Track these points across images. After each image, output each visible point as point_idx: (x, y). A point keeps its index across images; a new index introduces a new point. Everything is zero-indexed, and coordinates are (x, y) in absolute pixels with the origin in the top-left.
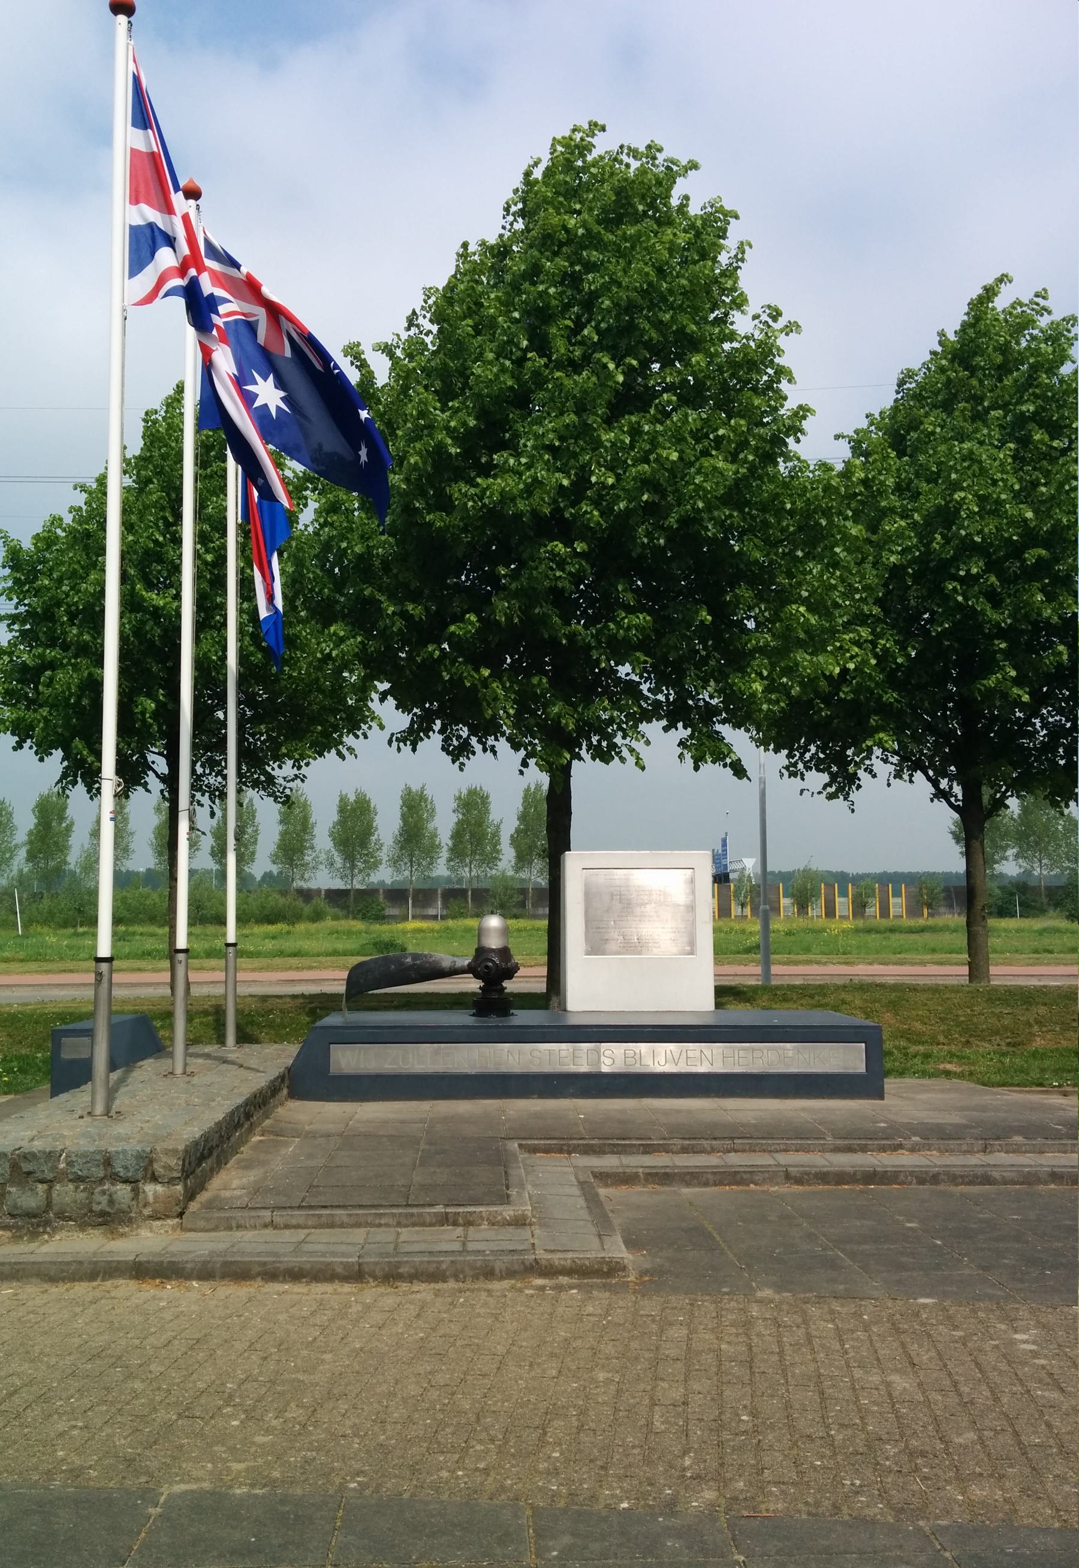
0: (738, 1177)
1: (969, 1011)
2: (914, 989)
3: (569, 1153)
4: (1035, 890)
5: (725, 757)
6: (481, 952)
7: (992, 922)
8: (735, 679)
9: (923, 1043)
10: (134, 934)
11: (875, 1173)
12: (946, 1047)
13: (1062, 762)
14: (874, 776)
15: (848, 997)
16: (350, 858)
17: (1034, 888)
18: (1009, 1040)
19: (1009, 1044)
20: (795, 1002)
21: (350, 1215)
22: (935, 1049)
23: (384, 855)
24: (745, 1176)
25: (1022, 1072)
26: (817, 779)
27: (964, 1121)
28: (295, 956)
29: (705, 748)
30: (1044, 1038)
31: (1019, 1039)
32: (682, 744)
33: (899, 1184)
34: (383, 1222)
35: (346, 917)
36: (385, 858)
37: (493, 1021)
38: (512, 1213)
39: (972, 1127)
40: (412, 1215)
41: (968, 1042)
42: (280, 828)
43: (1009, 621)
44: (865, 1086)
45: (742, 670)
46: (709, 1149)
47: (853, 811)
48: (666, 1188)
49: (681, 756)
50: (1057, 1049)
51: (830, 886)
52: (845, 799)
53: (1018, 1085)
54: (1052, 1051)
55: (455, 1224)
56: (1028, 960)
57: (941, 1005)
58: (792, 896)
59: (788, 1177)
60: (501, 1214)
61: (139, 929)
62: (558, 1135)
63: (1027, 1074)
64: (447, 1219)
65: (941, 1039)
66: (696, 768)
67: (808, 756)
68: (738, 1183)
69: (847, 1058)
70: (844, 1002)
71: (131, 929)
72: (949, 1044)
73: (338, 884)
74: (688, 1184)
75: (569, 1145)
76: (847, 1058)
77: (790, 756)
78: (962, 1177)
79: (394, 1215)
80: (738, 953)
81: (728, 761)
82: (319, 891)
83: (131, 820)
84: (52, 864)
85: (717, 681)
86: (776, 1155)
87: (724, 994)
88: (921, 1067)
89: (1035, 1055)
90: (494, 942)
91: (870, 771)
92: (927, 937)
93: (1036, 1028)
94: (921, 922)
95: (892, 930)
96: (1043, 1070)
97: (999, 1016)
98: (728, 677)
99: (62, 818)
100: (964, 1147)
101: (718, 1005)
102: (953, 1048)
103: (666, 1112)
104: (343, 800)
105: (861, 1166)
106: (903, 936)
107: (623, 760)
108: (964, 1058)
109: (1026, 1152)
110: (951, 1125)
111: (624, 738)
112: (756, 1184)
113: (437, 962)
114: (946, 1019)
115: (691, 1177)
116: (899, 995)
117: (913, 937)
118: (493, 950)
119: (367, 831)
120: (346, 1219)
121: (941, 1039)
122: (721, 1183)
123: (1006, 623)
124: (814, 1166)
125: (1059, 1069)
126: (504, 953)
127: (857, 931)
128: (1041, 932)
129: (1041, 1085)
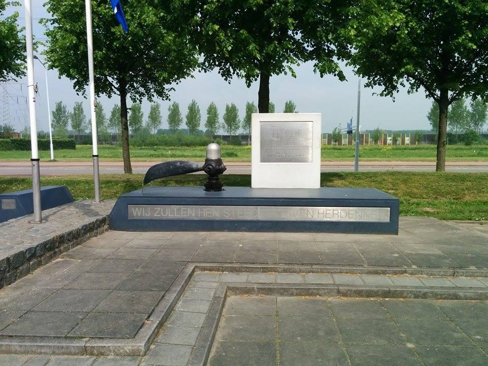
0: (310, 291)
1: (437, 184)
2: (414, 174)
3: (223, 271)
4: (454, 136)
5: (335, 70)
6: (208, 161)
7: (448, 146)
8: (342, 31)
9: (417, 198)
10: (159, 149)
11: (389, 291)
12: (427, 200)
13: (482, 81)
14: (404, 86)
15: (385, 178)
16: (230, 125)
17: (453, 135)
18: (454, 197)
19: (454, 199)
20: (364, 180)
21: (21, 346)
22: (422, 200)
23: (241, 124)
24: (314, 291)
25: (461, 212)
26: (380, 89)
27: (439, 252)
28: (200, 157)
29: (326, 68)
30: (470, 196)
31: (459, 196)
32: (315, 65)
33: (403, 298)
34: (43, 351)
35: (228, 144)
36: (241, 126)
37: (213, 194)
38: (130, 348)
39: (445, 258)
40: (62, 347)
41: (436, 197)
42: (208, 116)
43: (470, 12)
44: (390, 228)
45: (345, 27)
46: (298, 271)
47: (394, 101)
48: (269, 297)
49: (315, 71)
50: (476, 202)
51: (385, 135)
52: (391, 96)
53: (460, 219)
54: (473, 202)
55: (92, 354)
56: (458, 164)
57: (425, 181)
58: (373, 138)
59: (339, 292)
60: (123, 348)
61: (161, 147)
62: (220, 259)
63: (464, 213)
64: (86, 351)
65: (425, 196)
66: (322, 76)
67: (376, 79)
68: (311, 295)
69: (381, 215)
70: (384, 180)
71: (158, 147)
72: (428, 199)
73: (226, 134)
74: (282, 294)
75: (223, 267)
76: (381, 215)
77: (369, 79)
78: (440, 295)
79: (50, 347)
80: (351, 157)
81: (337, 73)
82: (220, 136)
83: (161, 112)
84: (137, 127)
85: (333, 33)
86: (335, 276)
87: (326, 178)
88: (415, 210)
89: (466, 204)
90: (214, 157)
91: (402, 84)
92: (417, 151)
93: (466, 192)
94: (415, 146)
95: (405, 149)
96: (470, 212)
97: (450, 186)
98: (337, 30)
99: (139, 112)
100: (442, 273)
101: (322, 186)
102: (430, 200)
103: (285, 243)
104: (227, 107)
105: (382, 286)
106: (409, 151)
107: (286, 73)
108: (435, 205)
109: (477, 276)
110: (433, 255)
111: (287, 62)
112: (320, 296)
113: (190, 165)
114: (427, 187)
115: (284, 291)
116: (407, 177)
117: (413, 151)
118: (212, 160)
119: (235, 116)
120: (18, 349)
121: (425, 196)
122: (300, 295)
123: (468, 12)
124: (354, 286)
125: (478, 211)
126: (219, 161)
127: (393, 149)
128: (456, 149)
129: (470, 219)
